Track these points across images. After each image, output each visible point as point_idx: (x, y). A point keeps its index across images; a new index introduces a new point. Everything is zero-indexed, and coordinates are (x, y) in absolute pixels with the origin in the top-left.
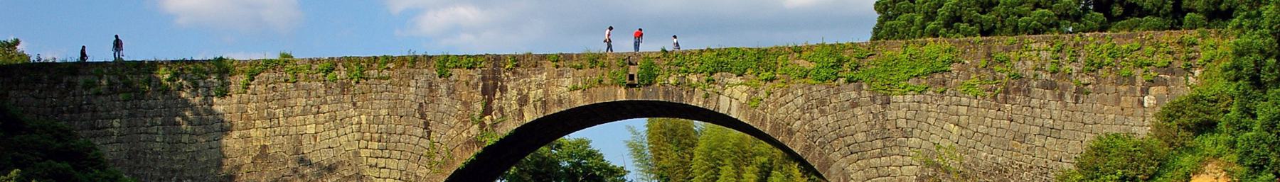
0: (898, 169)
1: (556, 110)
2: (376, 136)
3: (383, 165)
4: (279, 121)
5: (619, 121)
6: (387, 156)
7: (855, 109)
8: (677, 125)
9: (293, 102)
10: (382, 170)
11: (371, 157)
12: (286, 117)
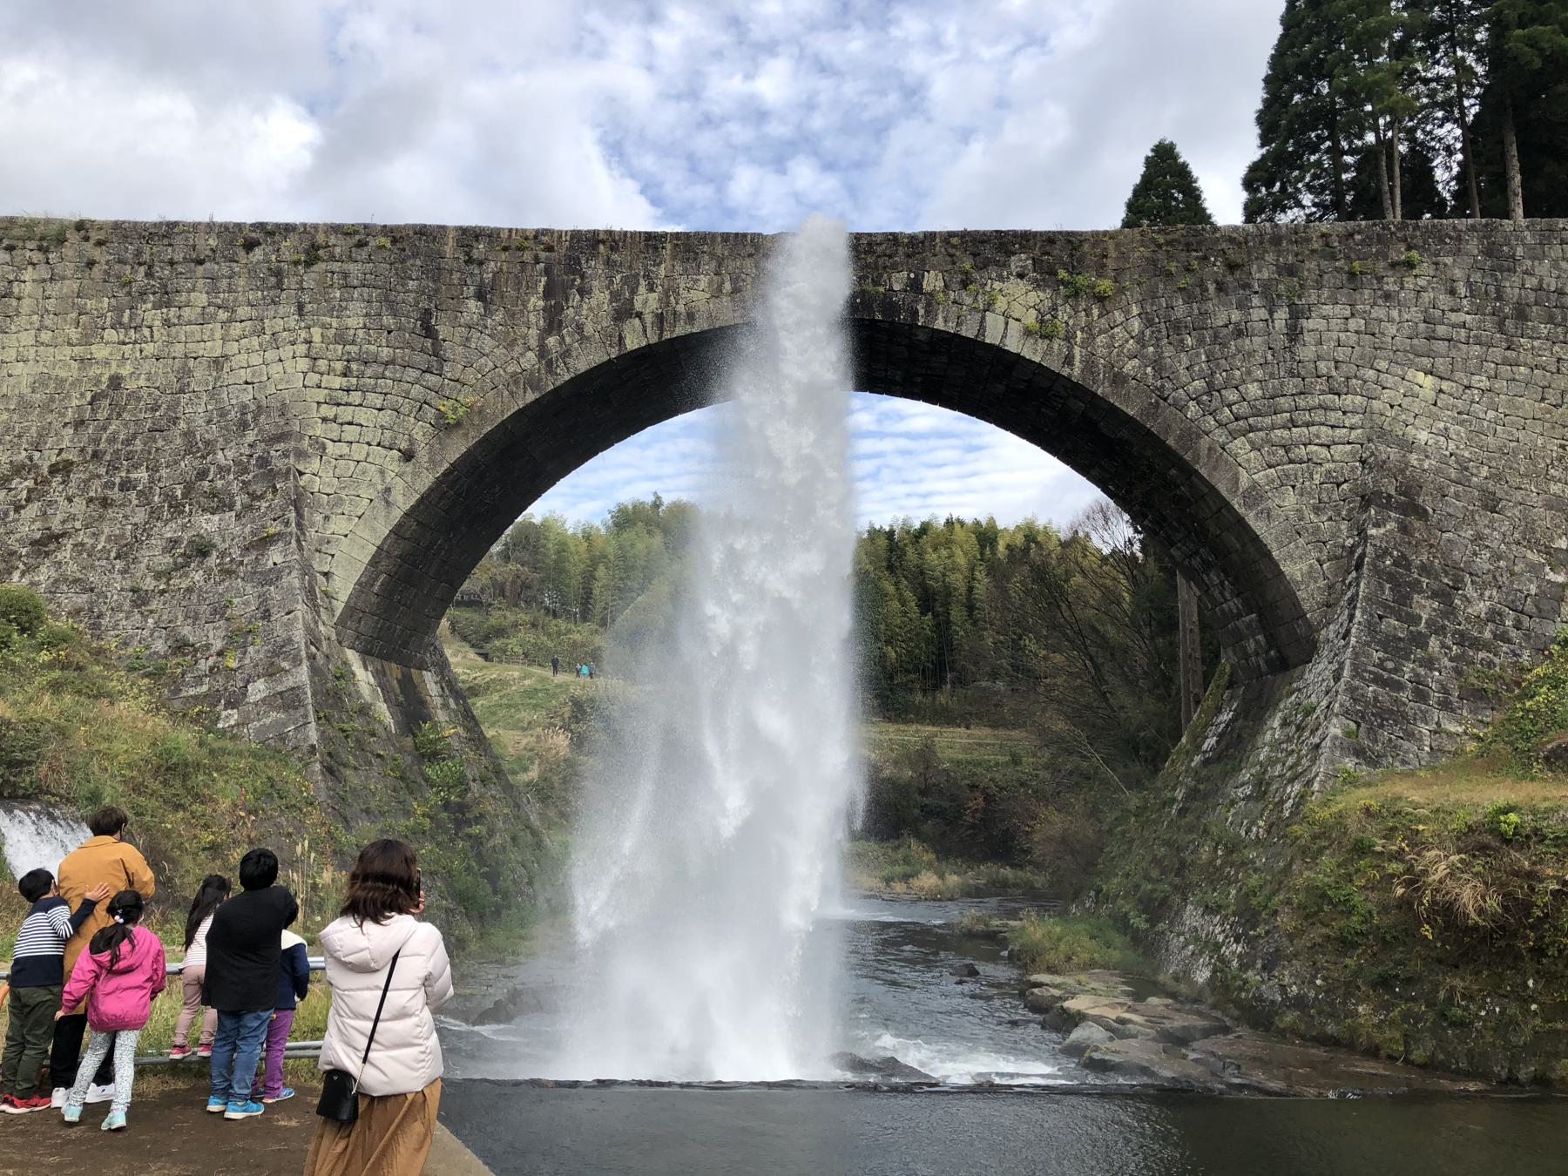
2: (339, 366)
3: (349, 419)
7: (218, 353)
9: (183, 297)
10: (346, 427)
12: (167, 323)
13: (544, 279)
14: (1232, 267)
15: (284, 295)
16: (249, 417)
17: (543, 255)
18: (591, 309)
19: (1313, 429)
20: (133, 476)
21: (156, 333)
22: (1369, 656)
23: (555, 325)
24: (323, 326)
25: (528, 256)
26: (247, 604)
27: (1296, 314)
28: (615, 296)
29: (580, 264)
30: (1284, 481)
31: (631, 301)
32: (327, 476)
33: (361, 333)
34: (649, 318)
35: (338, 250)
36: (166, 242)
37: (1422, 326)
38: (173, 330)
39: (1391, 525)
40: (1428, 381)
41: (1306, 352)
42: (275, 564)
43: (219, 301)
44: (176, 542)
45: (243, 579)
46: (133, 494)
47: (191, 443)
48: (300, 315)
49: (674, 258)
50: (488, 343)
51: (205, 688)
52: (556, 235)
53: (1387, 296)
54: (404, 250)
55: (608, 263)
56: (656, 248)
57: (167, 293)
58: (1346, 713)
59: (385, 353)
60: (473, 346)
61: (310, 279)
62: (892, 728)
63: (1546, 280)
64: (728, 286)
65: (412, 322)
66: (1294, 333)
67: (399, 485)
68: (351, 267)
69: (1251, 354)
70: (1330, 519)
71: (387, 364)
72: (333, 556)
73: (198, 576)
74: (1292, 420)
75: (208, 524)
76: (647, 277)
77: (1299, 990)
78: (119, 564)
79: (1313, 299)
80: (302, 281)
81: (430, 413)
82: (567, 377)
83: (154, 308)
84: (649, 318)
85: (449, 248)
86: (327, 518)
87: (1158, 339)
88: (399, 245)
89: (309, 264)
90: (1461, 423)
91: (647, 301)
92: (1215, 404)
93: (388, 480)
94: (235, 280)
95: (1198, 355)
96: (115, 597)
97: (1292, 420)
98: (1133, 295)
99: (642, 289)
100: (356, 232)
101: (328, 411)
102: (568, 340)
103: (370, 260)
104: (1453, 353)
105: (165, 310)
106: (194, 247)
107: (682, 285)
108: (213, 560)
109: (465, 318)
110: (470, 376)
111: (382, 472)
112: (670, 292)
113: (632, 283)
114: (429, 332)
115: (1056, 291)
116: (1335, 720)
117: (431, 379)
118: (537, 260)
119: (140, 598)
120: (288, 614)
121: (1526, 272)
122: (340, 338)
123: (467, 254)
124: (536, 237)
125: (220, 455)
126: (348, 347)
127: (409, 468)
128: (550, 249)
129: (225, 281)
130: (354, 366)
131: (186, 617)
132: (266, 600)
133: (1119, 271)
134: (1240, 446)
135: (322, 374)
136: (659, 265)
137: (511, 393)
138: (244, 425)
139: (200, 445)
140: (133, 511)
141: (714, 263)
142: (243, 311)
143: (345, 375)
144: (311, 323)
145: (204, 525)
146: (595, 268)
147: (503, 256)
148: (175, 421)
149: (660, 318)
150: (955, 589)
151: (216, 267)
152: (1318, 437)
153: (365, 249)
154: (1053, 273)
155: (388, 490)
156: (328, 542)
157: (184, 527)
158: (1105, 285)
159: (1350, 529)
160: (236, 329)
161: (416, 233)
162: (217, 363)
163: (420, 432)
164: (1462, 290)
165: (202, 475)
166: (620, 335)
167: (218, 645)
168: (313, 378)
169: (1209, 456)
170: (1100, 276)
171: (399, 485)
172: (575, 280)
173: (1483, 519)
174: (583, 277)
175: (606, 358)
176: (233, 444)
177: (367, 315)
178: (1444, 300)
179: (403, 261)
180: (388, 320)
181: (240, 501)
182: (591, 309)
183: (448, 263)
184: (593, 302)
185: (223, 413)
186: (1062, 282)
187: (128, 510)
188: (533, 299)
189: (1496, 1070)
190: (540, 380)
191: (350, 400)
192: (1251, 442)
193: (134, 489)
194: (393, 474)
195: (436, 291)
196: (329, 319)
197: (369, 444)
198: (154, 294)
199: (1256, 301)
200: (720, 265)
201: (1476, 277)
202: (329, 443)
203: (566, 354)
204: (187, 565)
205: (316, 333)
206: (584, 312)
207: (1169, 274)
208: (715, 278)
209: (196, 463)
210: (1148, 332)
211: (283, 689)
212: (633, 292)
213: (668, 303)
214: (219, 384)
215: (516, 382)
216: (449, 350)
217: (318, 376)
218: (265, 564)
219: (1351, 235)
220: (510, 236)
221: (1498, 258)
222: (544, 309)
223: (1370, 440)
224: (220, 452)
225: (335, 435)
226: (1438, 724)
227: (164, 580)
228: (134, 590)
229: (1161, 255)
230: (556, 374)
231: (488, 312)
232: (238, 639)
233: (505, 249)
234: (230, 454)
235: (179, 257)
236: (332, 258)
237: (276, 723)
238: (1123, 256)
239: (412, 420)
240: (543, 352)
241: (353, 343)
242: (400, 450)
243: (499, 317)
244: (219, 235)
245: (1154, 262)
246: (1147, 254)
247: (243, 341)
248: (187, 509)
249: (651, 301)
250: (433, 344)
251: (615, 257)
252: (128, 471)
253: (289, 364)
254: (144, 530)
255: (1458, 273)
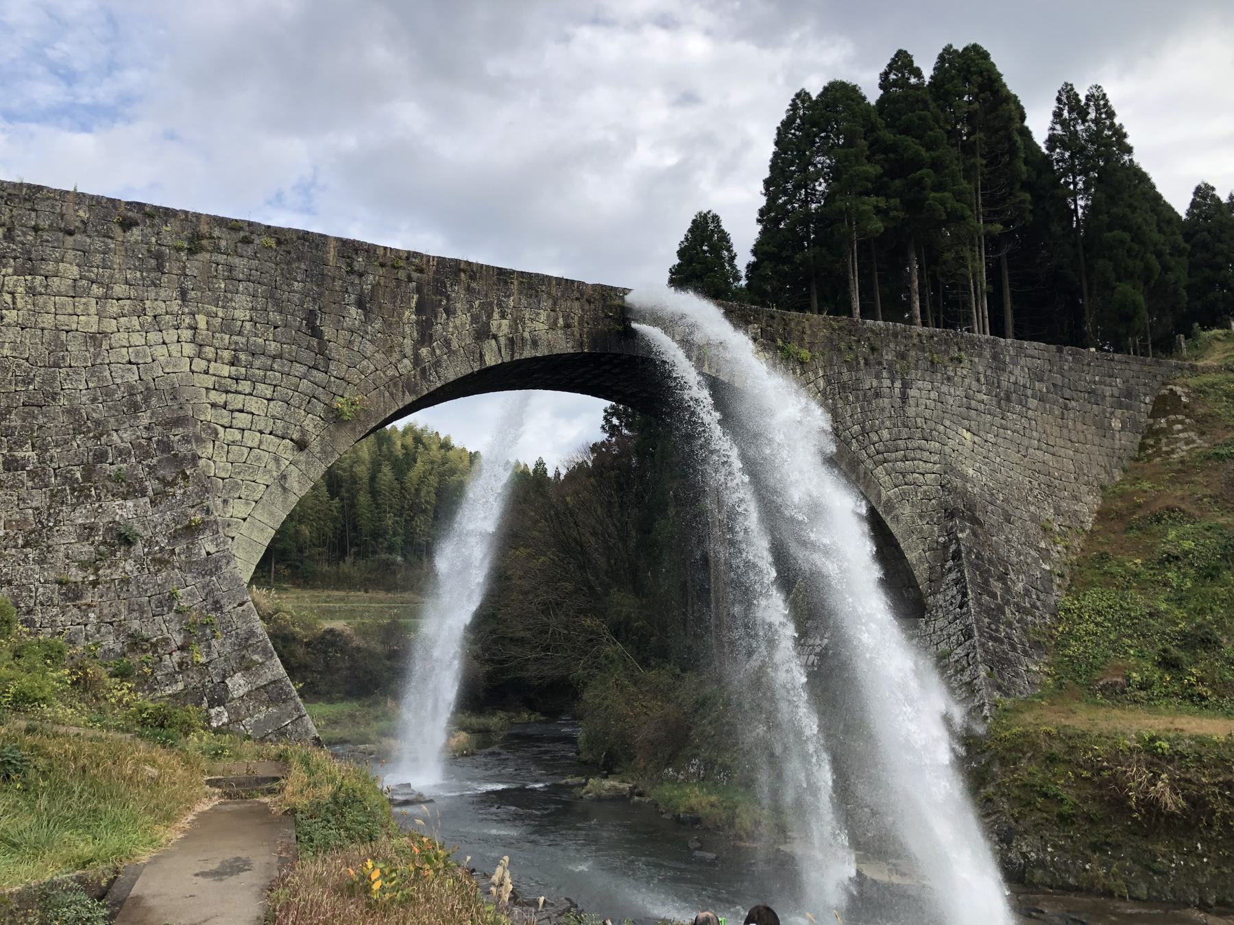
0: (921, 477)
1: (528, 353)
2: (226, 355)
3: (240, 406)
4: (14, 298)
5: (579, 395)
6: (247, 392)
7: (94, 329)
8: (1208, 592)
9: (51, 266)
10: (236, 414)
11: (214, 389)
12: (31, 291)
13: (416, 297)
14: (873, 349)
15: (165, 279)
16: (139, 398)
17: (415, 275)
18: (455, 327)
19: (916, 462)
20: (19, 454)
21: (19, 300)
22: (983, 622)
23: (427, 338)
24: (208, 314)
25: (402, 275)
26: (191, 594)
27: (905, 386)
28: (475, 319)
29: (445, 287)
30: (903, 496)
31: (488, 324)
32: (221, 460)
33: (248, 325)
34: (502, 341)
35: (223, 243)
36: (28, 205)
37: (965, 399)
38: (41, 300)
39: (968, 531)
40: (968, 435)
41: (911, 411)
42: (208, 554)
43: (93, 276)
44: (91, 529)
45: (180, 569)
46: (24, 476)
47: (78, 422)
48: (183, 300)
49: (520, 293)
50: (369, 349)
51: (180, 686)
52: (425, 259)
53: (949, 379)
54: (289, 252)
55: (469, 289)
56: (506, 283)
57: (30, 260)
58: (984, 661)
59: (273, 347)
60: (356, 349)
61: (193, 268)
62: (307, 594)
63: (1019, 378)
64: (561, 321)
65: (297, 321)
66: (904, 398)
67: (294, 472)
68: (237, 261)
69: (883, 410)
70: (928, 523)
71: (274, 357)
72: (233, 538)
73: (129, 566)
74: (905, 456)
75: (124, 511)
76: (499, 305)
77: (1037, 855)
78: (32, 554)
79: (913, 376)
80: (185, 267)
81: (320, 408)
82: (439, 385)
83: (15, 273)
84: (502, 341)
85: (332, 255)
86: (225, 502)
87: (834, 395)
88: (283, 247)
89: (192, 252)
90: (986, 464)
91: (500, 326)
92: (866, 442)
93: (283, 468)
94: (111, 256)
95: (856, 408)
96: (41, 590)
97: (905, 456)
98: (820, 362)
99: (496, 316)
100: (241, 229)
101: (215, 397)
102: (438, 352)
103: (255, 257)
104: (979, 419)
105: (29, 278)
106: (62, 216)
107: (527, 316)
108: (139, 549)
109: (348, 323)
110: (354, 375)
111: (277, 460)
112: (517, 321)
113: (488, 308)
114: (316, 332)
115: (775, 353)
116: (980, 667)
117: (319, 376)
118: (410, 279)
119: (72, 593)
120: (240, 605)
121: (1010, 372)
122: (227, 326)
123: (349, 265)
124: (407, 258)
125: (115, 436)
126: (235, 338)
127: (302, 457)
128: (421, 271)
129: (99, 257)
130: (243, 357)
131: (131, 611)
132: (211, 591)
133: (812, 344)
134: (880, 471)
135: (209, 361)
136: (509, 296)
137: (391, 394)
138: (135, 408)
139: (89, 424)
140: (29, 494)
141: (550, 302)
142: (119, 290)
143: (233, 364)
144: (195, 309)
145: (120, 512)
146: (457, 292)
147: (381, 271)
148: (54, 396)
149: (511, 342)
150: (361, 479)
151: (88, 240)
152: (918, 468)
153: (251, 246)
154: (774, 341)
155: (284, 477)
156: (229, 525)
157: (95, 513)
158: (805, 354)
159: (940, 530)
160: (113, 307)
161: (299, 238)
162: (94, 339)
163: (310, 423)
164: (983, 380)
165: (101, 457)
166: (481, 352)
167: (178, 639)
168: (200, 365)
169: (865, 478)
170: (801, 346)
171: (294, 472)
172: (441, 301)
173: (1007, 529)
174: (448, 298)
175: (470, 371)
176: (127, 425)
177: (252, 309)
178: (974, 384)
179: (289, 263)
180: (275, 317)
181: (151, 485)
182: (455, 327)
183: (330, 271)
184: (458, 322)
185: (108, 393)
186: (778, 348)
187: (23, 492)
188: (407, 313)
189: (1192, 899)
190: (416, 385)
191: (240, 388)
192: (886, 470)
193: (23, 469)
194: (288, 463)
195: (321, 294)
196: (214, 309)
197: (261, 432)
198: (15, 258)
199: (885, 374)
200: (555, 304)
201: (989, 372)
202: (221, 430)
203: (437, 364)
204: (113, 553)
205: (202, 320)
206: (451, 330)
207: (839, 350)
208: (552, 313)
209: (90, 444)
210: (828, 389)
211: (262, 682)
212: (490, 316)
213: (517, 329)
214: (99, 361)
215: (396, 385)
216: (334, 349)
217: (205, 363)
218: (199, 554)
219: (932, 337)
220: (385, 254)
221: (998, 364)
222: (417, 322)
223: (945, 473)
224: (115, 434)
225: (226, 421)
226: (1027, 666)
227: (91, 570)
228: (60, 583)
229: (835, 337)
230: (430, 381)
231: (367, 320)
232: (196, 632)
233: (382, 265)
234: (127, 436)
235: (44, 224)
236: (217, 249)
237: (268, 718)
238: (814, 334)
239: (303, 413)
240: (417, 360)
241: (240, 333)
242: (292, 440)
243: (378, 325)
244: (90, 207)
245: (831, 340)
246: (828, 335)
247: (122, 320)
248: (93, 493)
249: (503, 327)
250: (318, 343)
251: (474, 285)
252: (11, 449)
253: (174, 348)
254: (50, 514)
255: (981, 369)
